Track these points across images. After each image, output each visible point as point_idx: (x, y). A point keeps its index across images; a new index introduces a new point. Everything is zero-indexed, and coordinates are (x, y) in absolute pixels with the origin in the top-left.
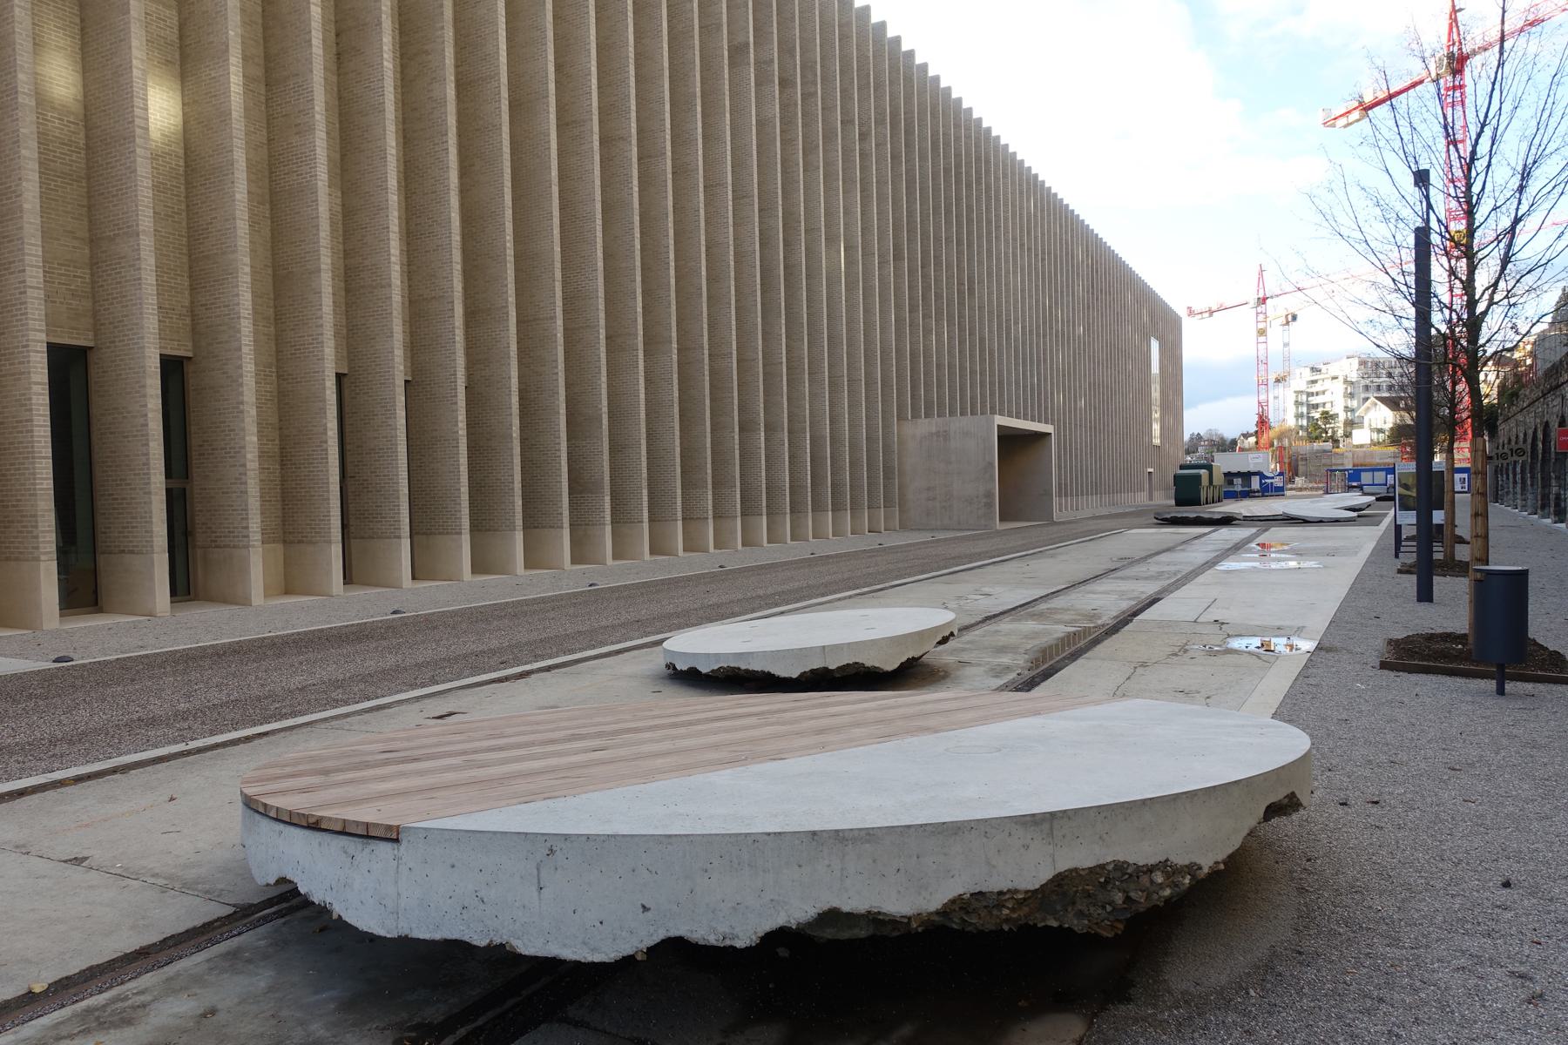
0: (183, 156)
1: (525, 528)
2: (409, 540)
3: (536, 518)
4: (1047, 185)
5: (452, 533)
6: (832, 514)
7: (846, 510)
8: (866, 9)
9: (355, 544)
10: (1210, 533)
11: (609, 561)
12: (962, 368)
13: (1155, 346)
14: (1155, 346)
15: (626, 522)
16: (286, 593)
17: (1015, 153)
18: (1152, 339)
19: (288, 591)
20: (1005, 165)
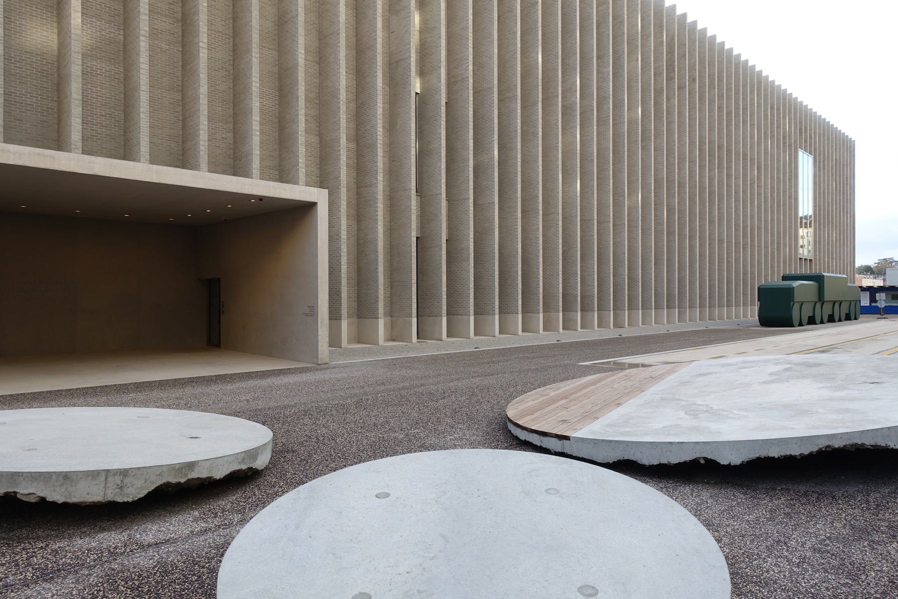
0: (232, 129)
1: (500, 313)
2: (416, 319)
3: (424, 310)
4: (835, 126)
5: (535, 313)
6: (655, 311)
7: (716, 307)
8: (673, 8)
9: (419, 317)
10: (594, 383)
11: (579, 329)
12: (832, 251)
13: (805, 164)
14: (805, 164)
15: (513, 313)
16: (358, 343)
17: (802, 102)
18: (801, 153)
19: (359, 342)
20: (720, 62)
